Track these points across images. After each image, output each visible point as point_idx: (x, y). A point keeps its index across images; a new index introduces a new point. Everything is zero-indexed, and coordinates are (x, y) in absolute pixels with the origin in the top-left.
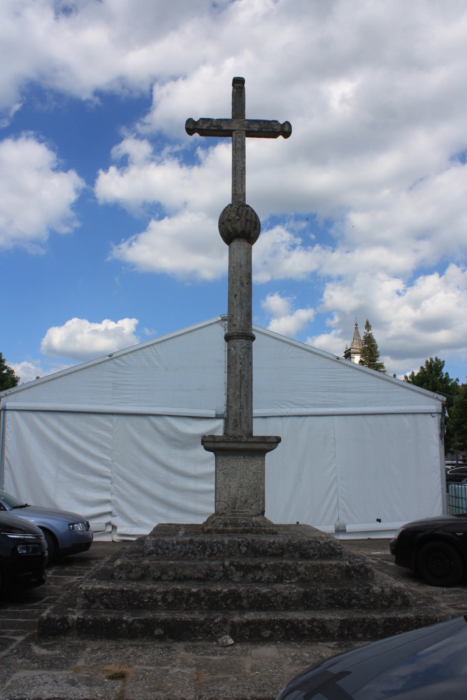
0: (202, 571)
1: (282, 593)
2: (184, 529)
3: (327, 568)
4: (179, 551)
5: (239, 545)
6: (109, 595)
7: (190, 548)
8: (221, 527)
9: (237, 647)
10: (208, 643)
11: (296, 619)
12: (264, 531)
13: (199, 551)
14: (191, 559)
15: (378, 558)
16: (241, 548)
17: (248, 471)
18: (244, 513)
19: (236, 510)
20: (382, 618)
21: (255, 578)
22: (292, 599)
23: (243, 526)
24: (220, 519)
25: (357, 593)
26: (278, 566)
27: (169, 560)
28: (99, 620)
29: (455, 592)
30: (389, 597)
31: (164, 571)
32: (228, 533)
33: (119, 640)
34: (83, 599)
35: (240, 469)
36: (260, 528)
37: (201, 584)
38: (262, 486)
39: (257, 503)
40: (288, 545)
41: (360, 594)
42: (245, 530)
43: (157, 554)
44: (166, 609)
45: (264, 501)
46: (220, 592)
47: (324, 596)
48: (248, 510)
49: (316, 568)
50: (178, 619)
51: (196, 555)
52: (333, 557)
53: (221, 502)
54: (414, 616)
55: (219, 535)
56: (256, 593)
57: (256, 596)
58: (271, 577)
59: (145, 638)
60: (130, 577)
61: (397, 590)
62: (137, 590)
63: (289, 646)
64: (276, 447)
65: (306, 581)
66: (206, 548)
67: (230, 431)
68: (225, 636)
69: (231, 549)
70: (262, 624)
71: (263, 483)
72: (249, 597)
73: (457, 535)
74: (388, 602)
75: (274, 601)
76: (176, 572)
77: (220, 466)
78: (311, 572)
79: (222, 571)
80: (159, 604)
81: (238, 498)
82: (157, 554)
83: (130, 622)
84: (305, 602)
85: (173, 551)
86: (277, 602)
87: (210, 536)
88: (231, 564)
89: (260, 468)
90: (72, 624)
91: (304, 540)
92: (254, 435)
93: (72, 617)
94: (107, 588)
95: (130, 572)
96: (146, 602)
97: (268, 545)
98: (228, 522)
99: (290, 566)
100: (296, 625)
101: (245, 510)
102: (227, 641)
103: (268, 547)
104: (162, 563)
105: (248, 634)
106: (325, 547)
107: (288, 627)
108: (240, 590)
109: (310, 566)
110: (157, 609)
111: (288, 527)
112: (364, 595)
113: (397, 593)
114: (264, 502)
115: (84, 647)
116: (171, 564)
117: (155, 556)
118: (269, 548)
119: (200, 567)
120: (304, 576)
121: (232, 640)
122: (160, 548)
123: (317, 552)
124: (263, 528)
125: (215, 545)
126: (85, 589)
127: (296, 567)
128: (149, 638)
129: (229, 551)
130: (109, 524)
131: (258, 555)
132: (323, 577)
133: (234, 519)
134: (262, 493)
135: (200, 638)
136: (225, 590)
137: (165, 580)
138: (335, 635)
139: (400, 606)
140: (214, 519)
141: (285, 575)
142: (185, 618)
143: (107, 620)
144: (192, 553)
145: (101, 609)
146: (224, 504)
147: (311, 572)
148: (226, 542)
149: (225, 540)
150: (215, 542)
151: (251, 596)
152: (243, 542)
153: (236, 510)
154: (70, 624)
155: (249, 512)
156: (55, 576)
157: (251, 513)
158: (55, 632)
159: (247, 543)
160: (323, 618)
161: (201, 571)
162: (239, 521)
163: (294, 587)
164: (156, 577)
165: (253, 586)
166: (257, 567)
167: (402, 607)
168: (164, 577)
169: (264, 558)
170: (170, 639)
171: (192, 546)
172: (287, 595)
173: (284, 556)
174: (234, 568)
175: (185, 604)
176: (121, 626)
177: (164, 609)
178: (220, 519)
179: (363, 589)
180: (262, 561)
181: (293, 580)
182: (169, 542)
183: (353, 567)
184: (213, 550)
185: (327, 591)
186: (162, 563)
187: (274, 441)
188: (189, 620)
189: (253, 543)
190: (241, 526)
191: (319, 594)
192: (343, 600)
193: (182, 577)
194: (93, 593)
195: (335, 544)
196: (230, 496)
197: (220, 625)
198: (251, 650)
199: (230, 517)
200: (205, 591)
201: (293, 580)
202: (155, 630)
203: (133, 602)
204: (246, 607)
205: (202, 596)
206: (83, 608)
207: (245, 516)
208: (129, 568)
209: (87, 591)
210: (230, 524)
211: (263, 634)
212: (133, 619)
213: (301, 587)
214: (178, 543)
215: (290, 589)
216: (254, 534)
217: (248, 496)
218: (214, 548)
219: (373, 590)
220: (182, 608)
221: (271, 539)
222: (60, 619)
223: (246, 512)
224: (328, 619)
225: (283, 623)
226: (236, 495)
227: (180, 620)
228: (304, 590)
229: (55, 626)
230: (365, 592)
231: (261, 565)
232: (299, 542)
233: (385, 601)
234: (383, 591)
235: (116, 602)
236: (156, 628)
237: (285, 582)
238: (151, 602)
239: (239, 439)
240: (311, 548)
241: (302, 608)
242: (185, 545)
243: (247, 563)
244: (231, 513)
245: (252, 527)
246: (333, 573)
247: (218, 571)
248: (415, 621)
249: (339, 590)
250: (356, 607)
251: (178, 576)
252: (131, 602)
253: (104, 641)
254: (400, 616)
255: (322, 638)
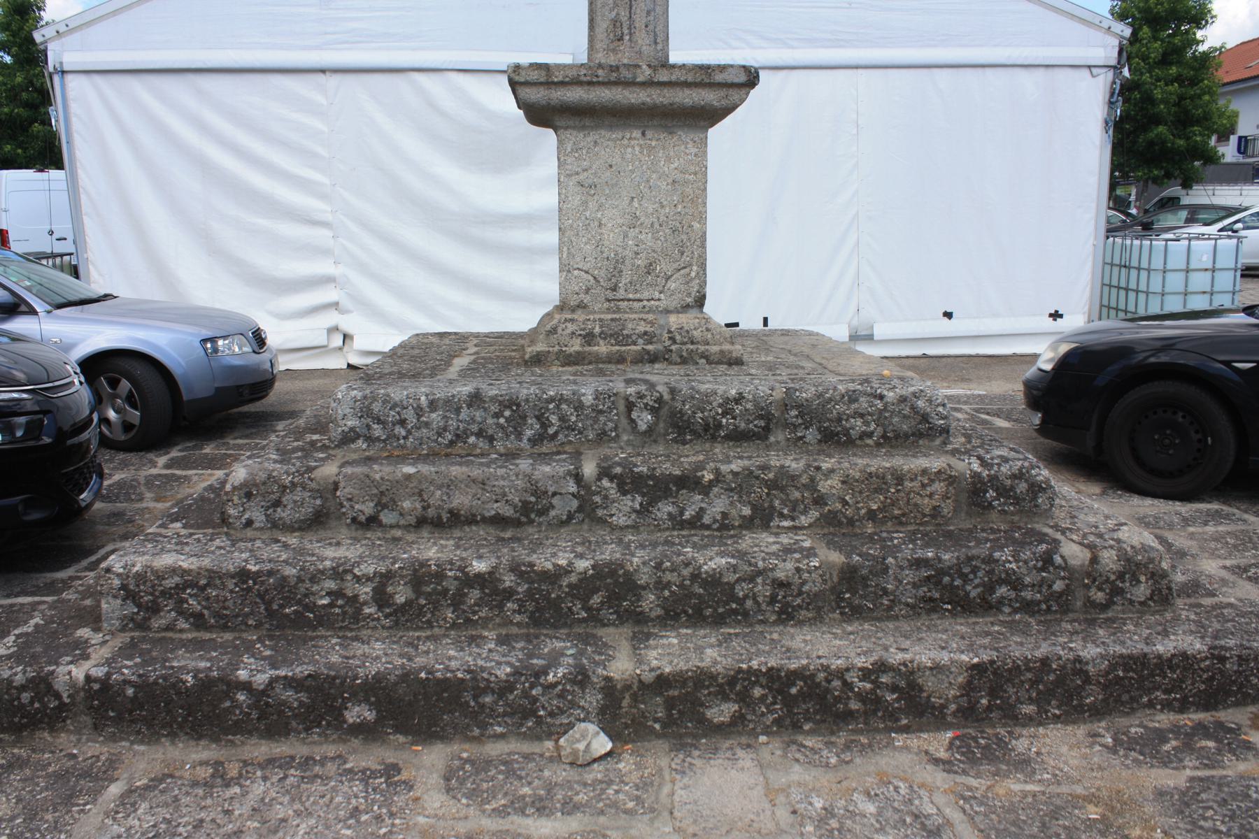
0: (510, 497)
1: (772, 570)
2: (475, 349)
3: (912, 480)
4: (439, 427)
5: (630, 406)
6: (203, 589)
7: (473, 420)
8: (576, 346)
9: (621, 766)
10: (526, 747)
11: (822, 665)
12: (704, 356)
13: (502, 427)
14: (479, 451)
15: (963, 407)
16: (634, 415)
17: (654, 176)
18: (645, 303)
19: (621, 293)
20: (1102, 656)
21: (682, 514)
22: (806, 588)
23: (640, 341)
24: (572, 320)
25: (1013, 566)
26: (757, 478)
27: (403, 459)
28: (156, 683)
29: (1216, 516)
30: (1113, 577)
31: (385, 500)
32: (599, 364)
33: (232, 741)
34: (119, 601)
35: (632, 171)
36: (692, 347)
37: (508, 535)
38: (699, 222)
39: (682, 272)
40: (785, 406)
41: (1024, 571)
42: (648, 352)
43: (370, 439)
44: (390, 628)
45: (703, 266)
46: (567, 571)
47: (909, 576)
48: (657, 293)
49: (876, 482)
50: (423, 675)
51: (491, 439)
52: (921, 442)
53: (576, 272)
54: (1205, 648)
55: (570, 369)
56: (686, 572)
57: (688, 582)
58: (734, 512)
59: (316, 733)
60: (280, 519)
61: (1140, 558)
62: (290, 571)
63: (798, 756)
64: (742, 101)
65: (845, 521)
66: (524, 418)
67: (600, 55)
68: (583, 725)
69: (602, 419)
70: (707, 683)
71: (700, 212)
72: (660, 585)
73: (1237, 370)
74: (1108, 591)
75: (746, 597)
76: (423, 500)
77: (569, 161)
78: (861, 492)
79: (573, 495)
80: (367, 611)
81: (624, 258)
82: (370, 439)
83: (262, 687)
84: (847, 596)
85: (419, 428)
86: (754, 598)
87: (541, 375)
88: (604, 473)
89: (692, 169)
90: (69, 696)
91: (835, 389)
92: (718, 310)
93: (70, 673)
94: (192, 567)
95: (277, 504)
96: (324, 605)
97: (720, 405)
98: (597, 330)
99: (793, 478)
100: (823, 683)
101: (646, 295)
102: (589, 745)
103: (720, 411)
104: (380, 471)
105: (660, 715)
106: (900, 412)
107: (794, 691)
108: (632, 563)
109: (857, 475)
110: (363, 626)
111: (764, 338)
112: (1035, 571)
113: (1138, 565)
114: (705, 270)
115: (106, 775)
116: (408, 477)
117: (364, 446)
118: (724, 414)
119: (502, 483)
120: (839, 506)
121: (607, 739)
122: (379, 421)
123: (873, 426)
124: (702, 348)
125: (551, 406)
126: (121, 570)
127: (812, 479)
128: (328, 732)
129: (596, 427)
130: (334, 330)
131: (688, 437)
132: (900, 509)
133: (612, 320)
134: (699, 242)
135: (499, 729)
136: (583, 565)
137: (392, 527)
138: (949, 712)
139: (1142, 603)
140: (555, 322)
141: (777, 503)
142: (447, 669)
143: (184, 682)
144: (479, 434)
145: (181, 631)
146: (585, 276)
147: (861, 492)
148: (588, 399)
149: (583, 391)
150: (551, 400)
151: (669, 582)
152: (641, 396)
153: (621, 293)
154: (65, 695)
155: (659, 300)
156: (169, 472)
157: (663, 304)
158: (16, 720)
159: (655, 401)
160: (911, 662)
161: (504, 495)
162: (630, 326)
163: (807, 544)
164: (362, 518)
165: (674, 544)
166: (689, 482)
167: (1150, 606)
168: (387, 517)
169: (708, 445)
170: (398, 736)
171: (478, 414)
172: (787, 576)
173: (772, 439)
174: (614, 485)
175: (452, 609)
176: (233, 700)
177: (383, 627)
178: (572, 320)
179: (1034, 554)
180: (701, 458)
181: (804, 520)
182: (405, 403)
183: (993, 478)
184: (545, 425)
185: (918, 563)
186: (380, 471)
187: (736, 80)
188: (460, 675)
189: (673, 399)
190: (635, 343)
191: (891, 572)
192: (969, 588)
193: (445, 517)
194: (149, 584)
195: (930, 401)
196: (602, 252)
197: (564, 690)
198: (673, 782)
199: (602, 316)
200: (515, 568)
201: (803, 518)
202: (346, 708)
203: (282, 606)
204: (653, 615)
205: (508, 584)
206: (123, 629)
207: (648, 312)
208: (273, 493)
209: (128, 577)
210: (603, 335)
211: (709, 713)
212: (271, 677)
213: (831, 544)
214: (433, 405)
215: (797, 556)
216: (676, 364)
217: (654, 251)
218: (547, 419)
219: (1062, 557)
220: (442, 623)
221: (726, 385)
222: (30, 681)
223: (648, 300)
224: (929, 665)
225: (777, 680)
226: (620, 250)
227: (427, 678)
228: (843, 559)
229: (16, 703)
230: (1040, 564)
231: (699, 474)
232: (820, 395)
233: (1100, 589)
234: (1094, 560)
235: (225, 608)
236: (349, 705)
237: (778, 527)
238: (340, 607)
239: (626, 74)
240: (855, 413)
241: (837, 615)
242: (458, 411)
243: (654, 469)
244: (606, 305)
245: (668, 343)
246: (931, 496)
247: (561, 494)
248: (1207, 663)
249: (958, 558)
250: (1007, 610)
251: (431, 512)
252: (275, 607)
253: (181, 745)
254: (1160, 648)
255: (904, 722)
